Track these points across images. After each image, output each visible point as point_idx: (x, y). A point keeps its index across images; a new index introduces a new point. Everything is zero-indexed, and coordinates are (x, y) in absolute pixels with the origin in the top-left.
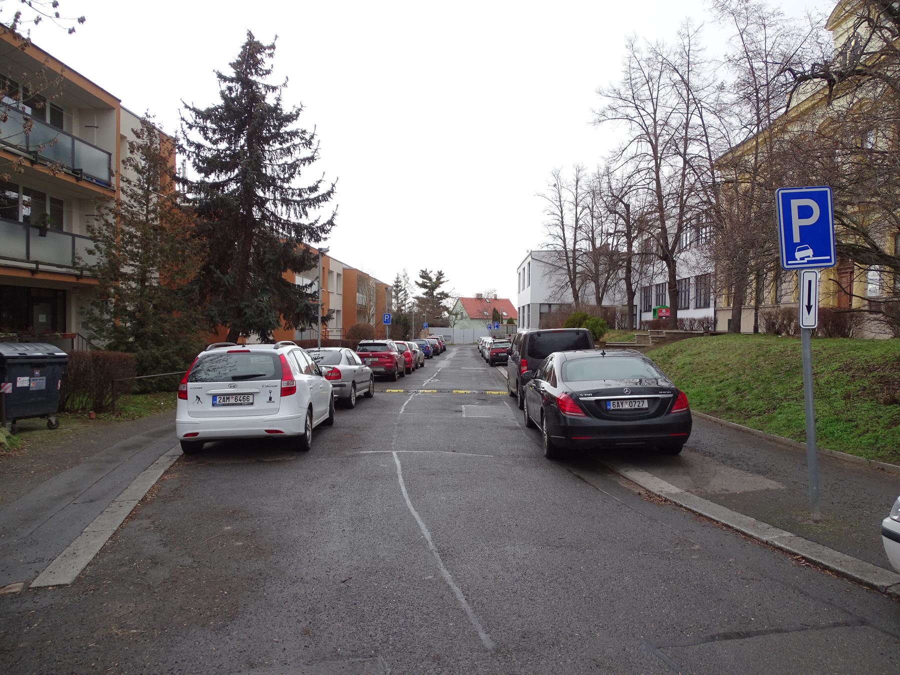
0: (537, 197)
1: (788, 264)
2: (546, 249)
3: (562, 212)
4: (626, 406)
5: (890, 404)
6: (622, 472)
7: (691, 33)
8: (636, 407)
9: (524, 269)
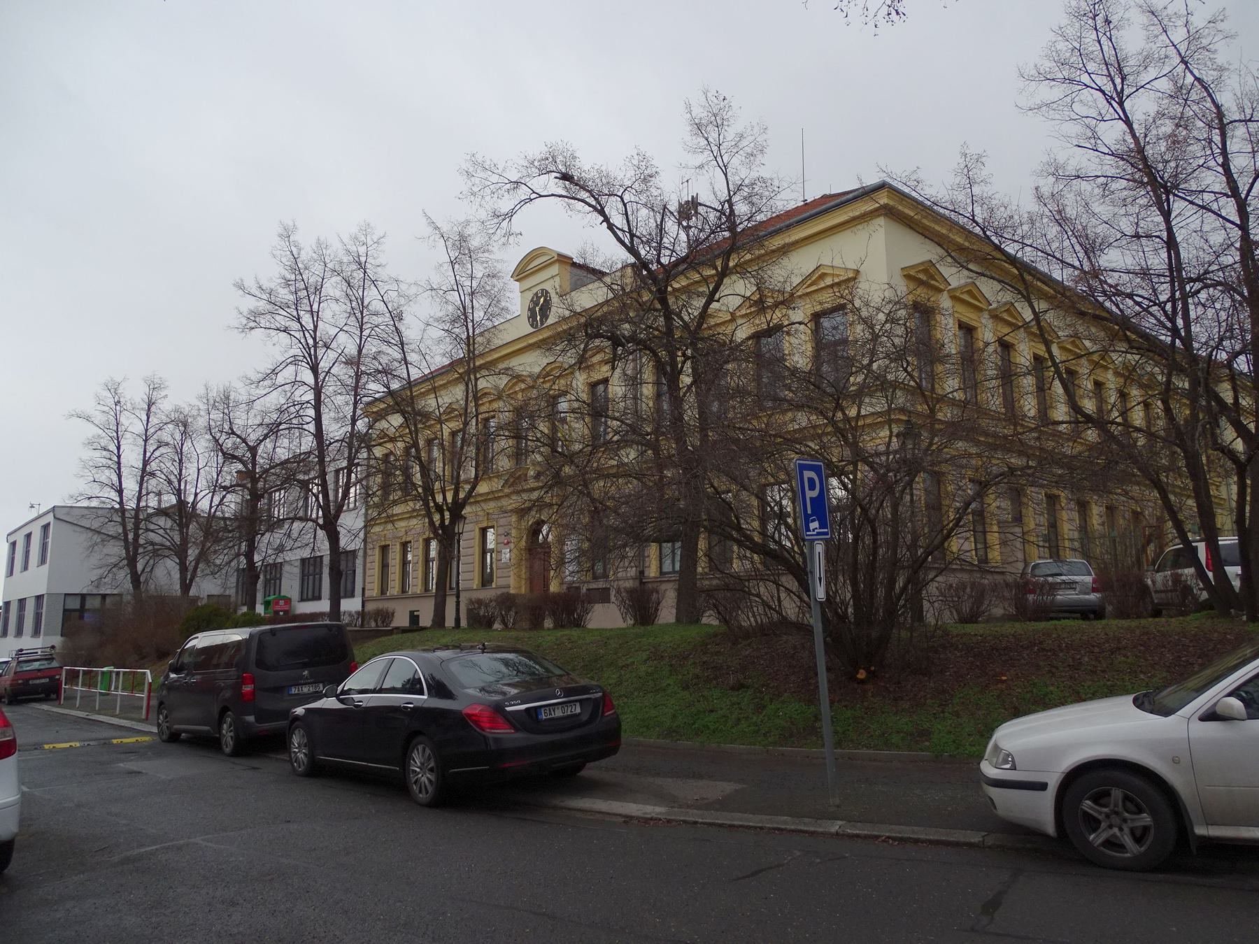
0: (75, 419)
1: (807, 535)
2: (85, 504)
3: (118, 448)
4: (558, 713)
5: (738, 690)
6: (556, 802)
7: (370, 243)
8: (569, 713)
9: (29, 536)
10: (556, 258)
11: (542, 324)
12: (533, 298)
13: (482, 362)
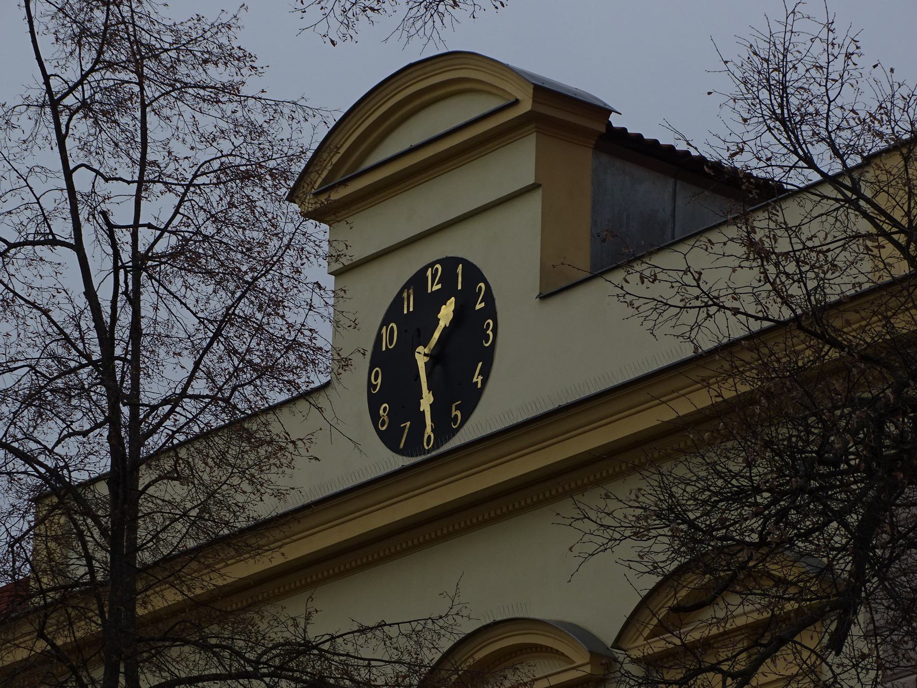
10: (526, 106)
11: (444, 429)
12: (398, 302)
13: (172, 597)
